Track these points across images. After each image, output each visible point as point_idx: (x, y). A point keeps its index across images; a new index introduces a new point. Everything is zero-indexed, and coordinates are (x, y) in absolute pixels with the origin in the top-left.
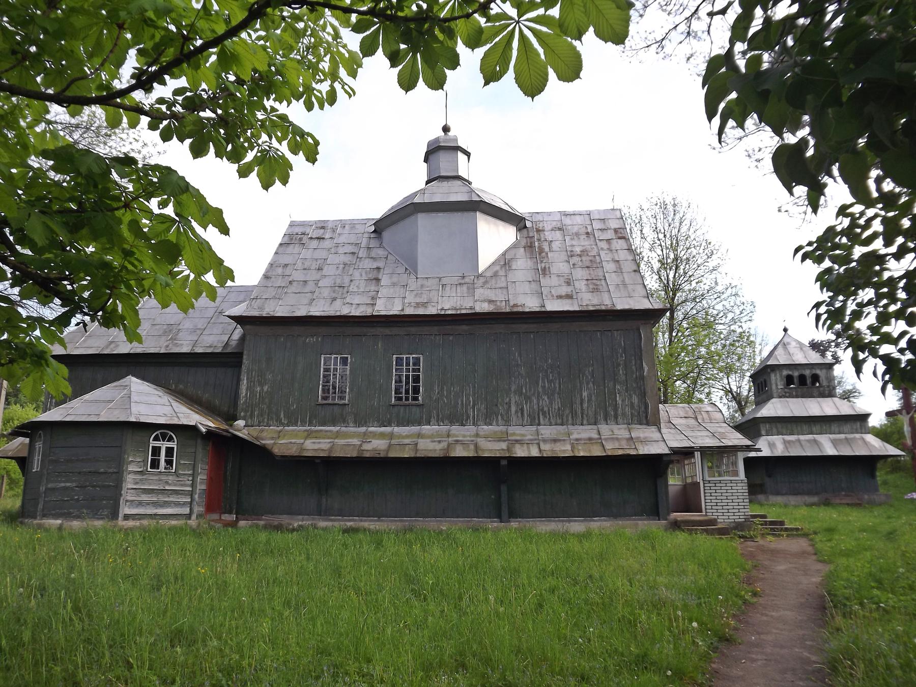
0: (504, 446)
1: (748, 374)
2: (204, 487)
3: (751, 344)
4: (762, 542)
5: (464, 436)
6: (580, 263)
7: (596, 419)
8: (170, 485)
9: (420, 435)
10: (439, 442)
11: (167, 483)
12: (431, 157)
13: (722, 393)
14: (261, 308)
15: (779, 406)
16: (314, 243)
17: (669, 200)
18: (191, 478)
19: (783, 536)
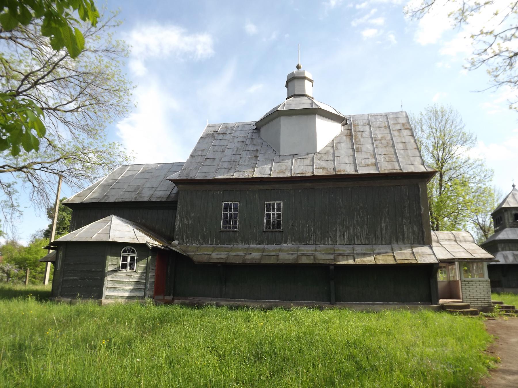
0: (332, 257)
1: (490, 213)
2: (153, 280)
3: (490, 195)
4: (500, 320)
5: (308, 251)
6: (380, 145)
7: (390, 240)
8: (132, 278)
9: (280, 250)
10: (292, 254)
11: (130, 277)
12: (289, 84)
13: (473, 225)
14: (188, 175)
15: (510, 232)
16: (221, 137)
17: (439, 109)
18: (145, 275)
19: (514, 316)
